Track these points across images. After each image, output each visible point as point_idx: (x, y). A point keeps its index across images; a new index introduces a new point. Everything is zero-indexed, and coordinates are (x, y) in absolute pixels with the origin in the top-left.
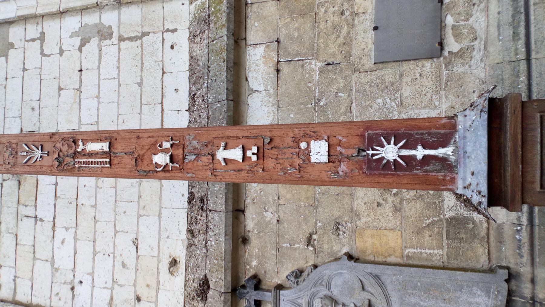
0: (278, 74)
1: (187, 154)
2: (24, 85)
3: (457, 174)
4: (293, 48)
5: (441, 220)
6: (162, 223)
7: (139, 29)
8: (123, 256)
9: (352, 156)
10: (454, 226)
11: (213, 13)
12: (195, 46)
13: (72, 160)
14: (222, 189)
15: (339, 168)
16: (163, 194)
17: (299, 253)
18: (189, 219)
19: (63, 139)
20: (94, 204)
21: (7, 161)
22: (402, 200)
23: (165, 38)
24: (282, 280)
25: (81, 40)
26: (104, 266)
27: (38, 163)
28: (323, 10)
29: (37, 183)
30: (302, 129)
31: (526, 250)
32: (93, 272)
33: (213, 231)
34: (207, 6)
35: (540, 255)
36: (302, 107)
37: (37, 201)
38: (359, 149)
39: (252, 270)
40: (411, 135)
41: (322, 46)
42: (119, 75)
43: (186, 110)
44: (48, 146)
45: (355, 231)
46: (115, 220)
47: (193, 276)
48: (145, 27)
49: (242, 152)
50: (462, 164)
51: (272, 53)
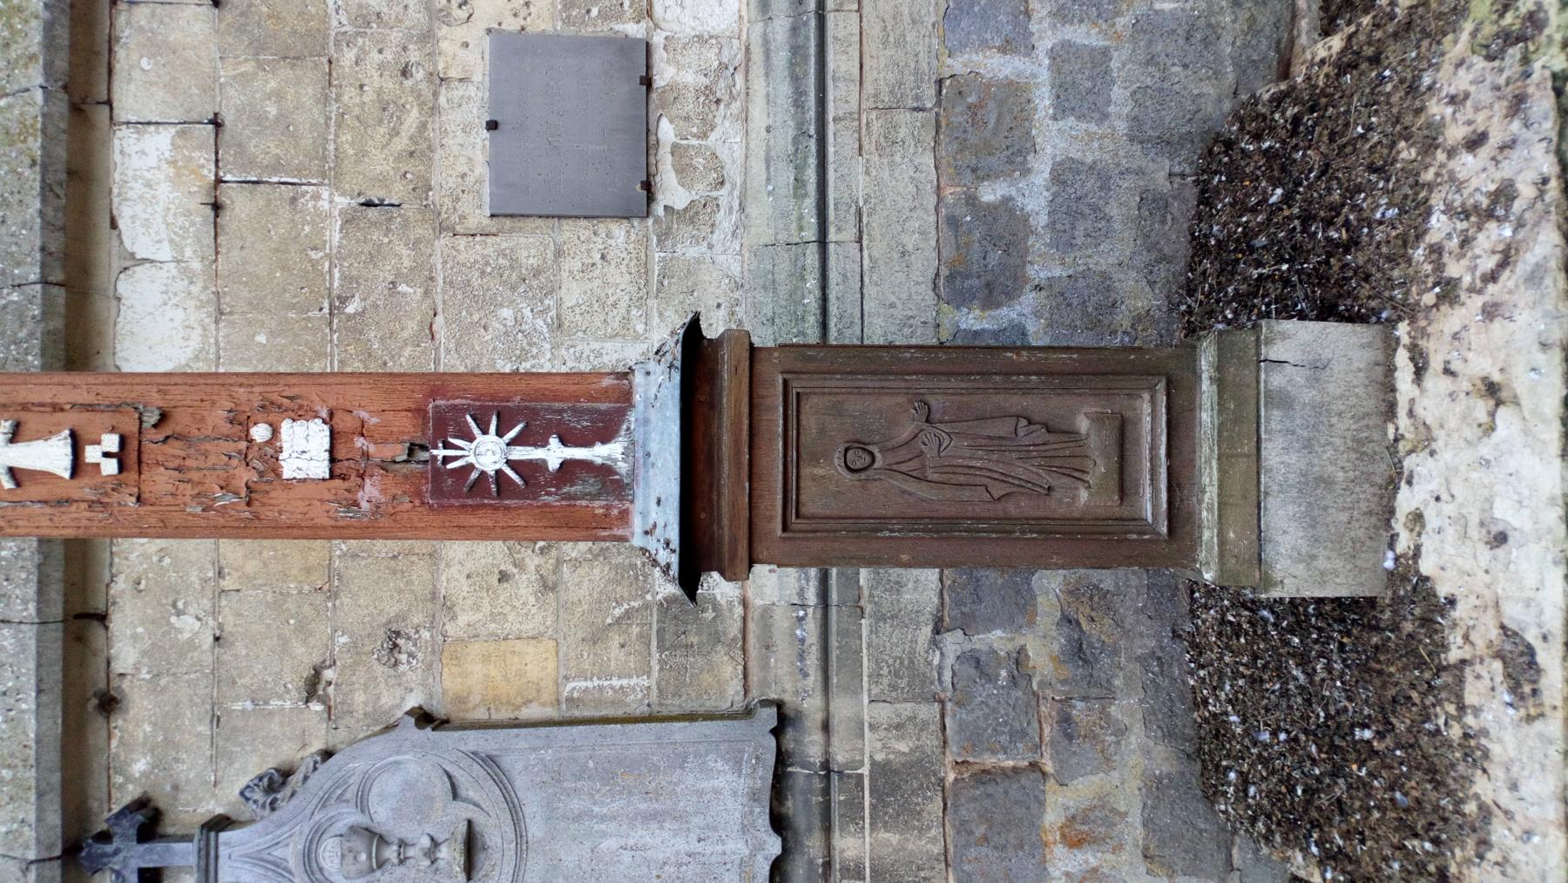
0: (217, 216)
3: (632, 502)
4: (264, 147)
5: (647, 606)
10: (675, 617)
14: (27, 553)
15: (360, 494)
22: (559, 562)
28: (349, 55)
30: (257, 389)
31: (813, 659)
35: (839, 670)
36: (291, 315)
40: (535, 412)
41: (351, 152)
45: (442, 650)
49: (69, 450)
50: (640, 478)
51: (196, 154)
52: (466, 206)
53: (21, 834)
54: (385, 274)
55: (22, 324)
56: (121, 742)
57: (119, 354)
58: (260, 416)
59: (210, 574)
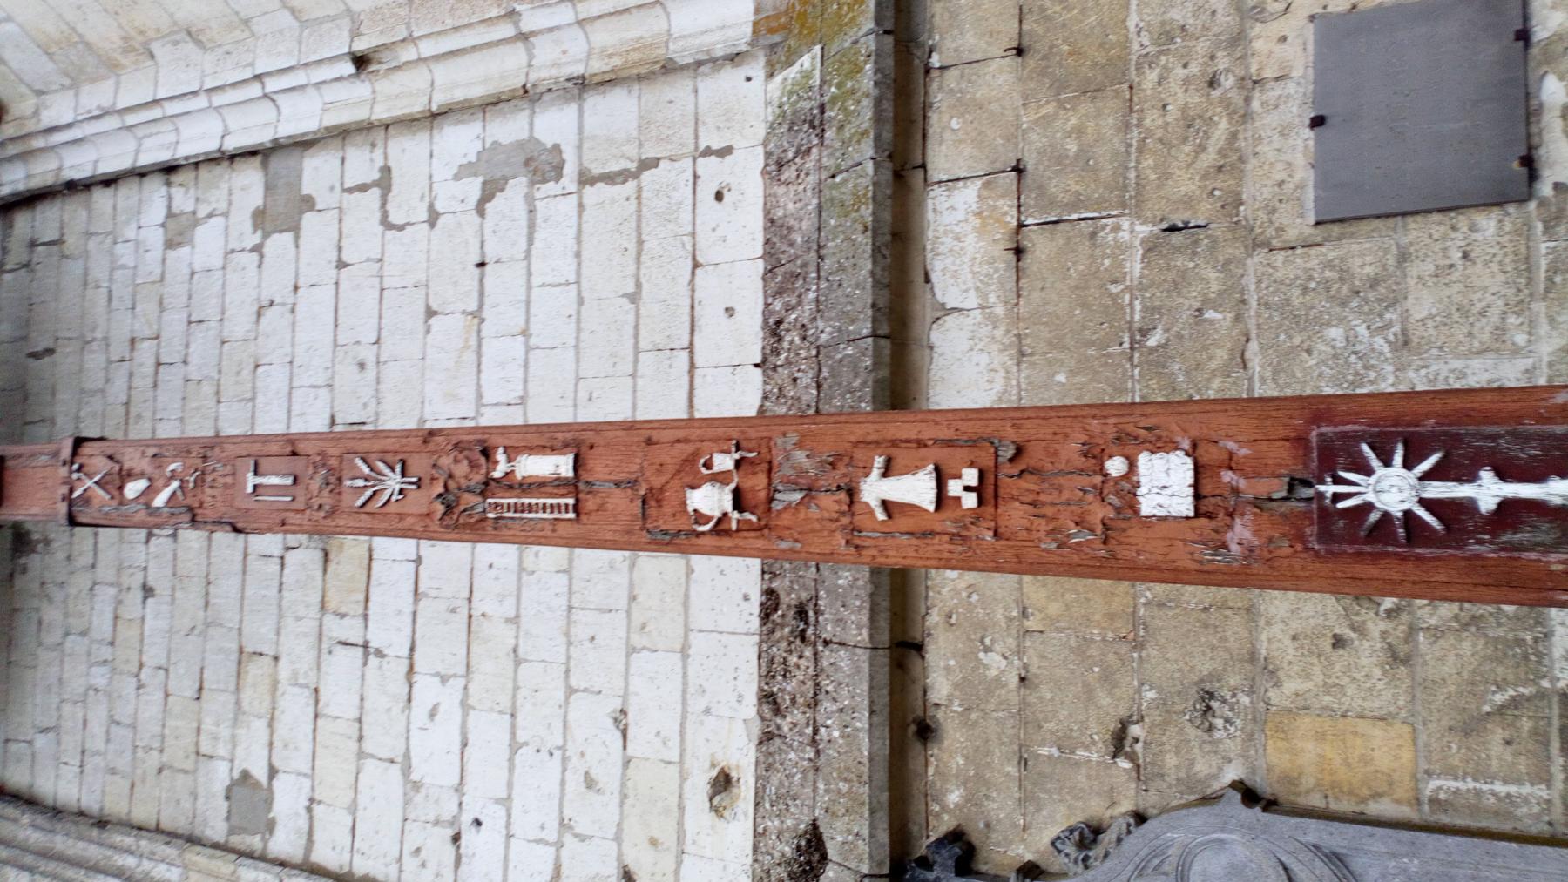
0: (1018, 260)
1: (780, 487)
2: (340, 306)
4: (1062, 186)
5: (1542, 695)
6: (691, 672)
7: (632, 151)
8: (587, 757)
9: (1271, 500)
11: (834, 99)
12: (781, 190)
13: (479, 499)
14: (860, 583)
15: (1229, 535)
16: (692, 593)
17: (1089, 777)
19: (456, 445)
21: (316, 502)
22: (1413, 630)
23: (699, 173)
25: (484, 183)
26: (538, 783)
27: (391, 508)
28: (1152, 76)
29: (371, 559)
30: (1112, 420)
32: (509, 797)
33: (835, 700)
34: (816, 80)
36: (1091, 352)
37: (370, 604)
38: (1293, 479)
39: (946, 817)
40: (1456, 439)
41: (1153, 177)
42: (578, 273)
43: (757, 365)
44: (419, 464)
45: (1262, 720)
46: (569, 658)
47: (777, 823)
48: (647, 145)
49: (933, 484)
51: (1000, 202)
52: (1282, 218)
53: (856, 846)
54: (1191, 299)
56: (937, 772)
58: (1115, 449)
59: (1015, 613)
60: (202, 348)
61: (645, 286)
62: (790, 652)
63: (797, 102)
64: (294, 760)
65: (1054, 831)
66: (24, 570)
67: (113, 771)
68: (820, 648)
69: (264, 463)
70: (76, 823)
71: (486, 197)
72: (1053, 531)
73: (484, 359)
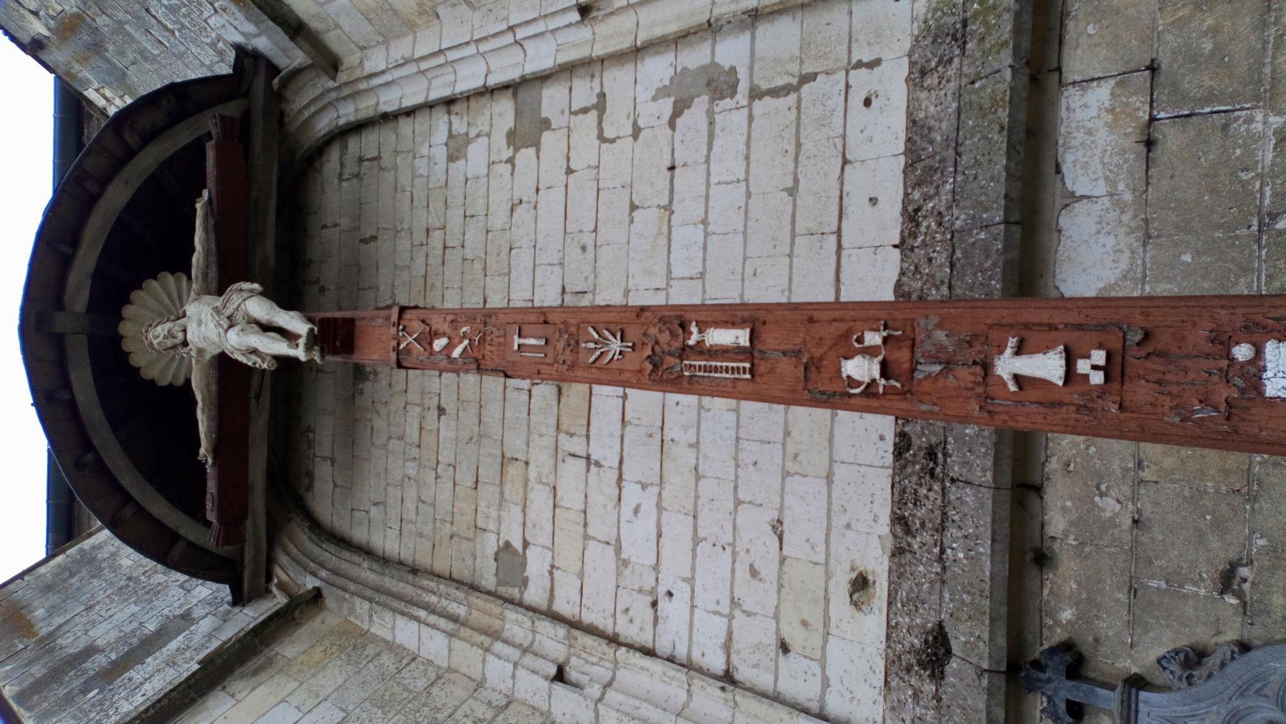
0: (1149, 151)
6: (834, 495)
7: (794, 68)
11: (976, 15)
12: (923, 95)
13: (678, 361)
14: (986, 433)
16: (836, 431)
17: (1196, 608)
18: (896, 494)
19: (660, 319)
20: (694, 441)
21: (561, 359)
23: (851, 83)
24: (1143, 666)
25: (675, 103)
26: (714, 568)
27: (614, 365)
30: (1240, 311)
32: (693, 577)
33: (960, 528)
36: (1219, 234)
39: (1059, 630)
42: (747, 172)
43: (895, 246)
44: (634, 332)
46: (737, 477)
47: (907, 620)
49: (1063, 362)
55: (988, 257)
57: (1058, 277)
59: (1131, 465)
60: (474, 236)
61: (802, 181)
62: (921, 485)
63: (941, 18)
64: (540, 537)
65: (1162, 651)
66: (362, 393)
67: (421, 535)
68: (948, 484)
69: (525, 329)
70: (398, 570)
71: (677, 112)
72: (1177, 407)
73: (673, 243)
